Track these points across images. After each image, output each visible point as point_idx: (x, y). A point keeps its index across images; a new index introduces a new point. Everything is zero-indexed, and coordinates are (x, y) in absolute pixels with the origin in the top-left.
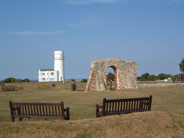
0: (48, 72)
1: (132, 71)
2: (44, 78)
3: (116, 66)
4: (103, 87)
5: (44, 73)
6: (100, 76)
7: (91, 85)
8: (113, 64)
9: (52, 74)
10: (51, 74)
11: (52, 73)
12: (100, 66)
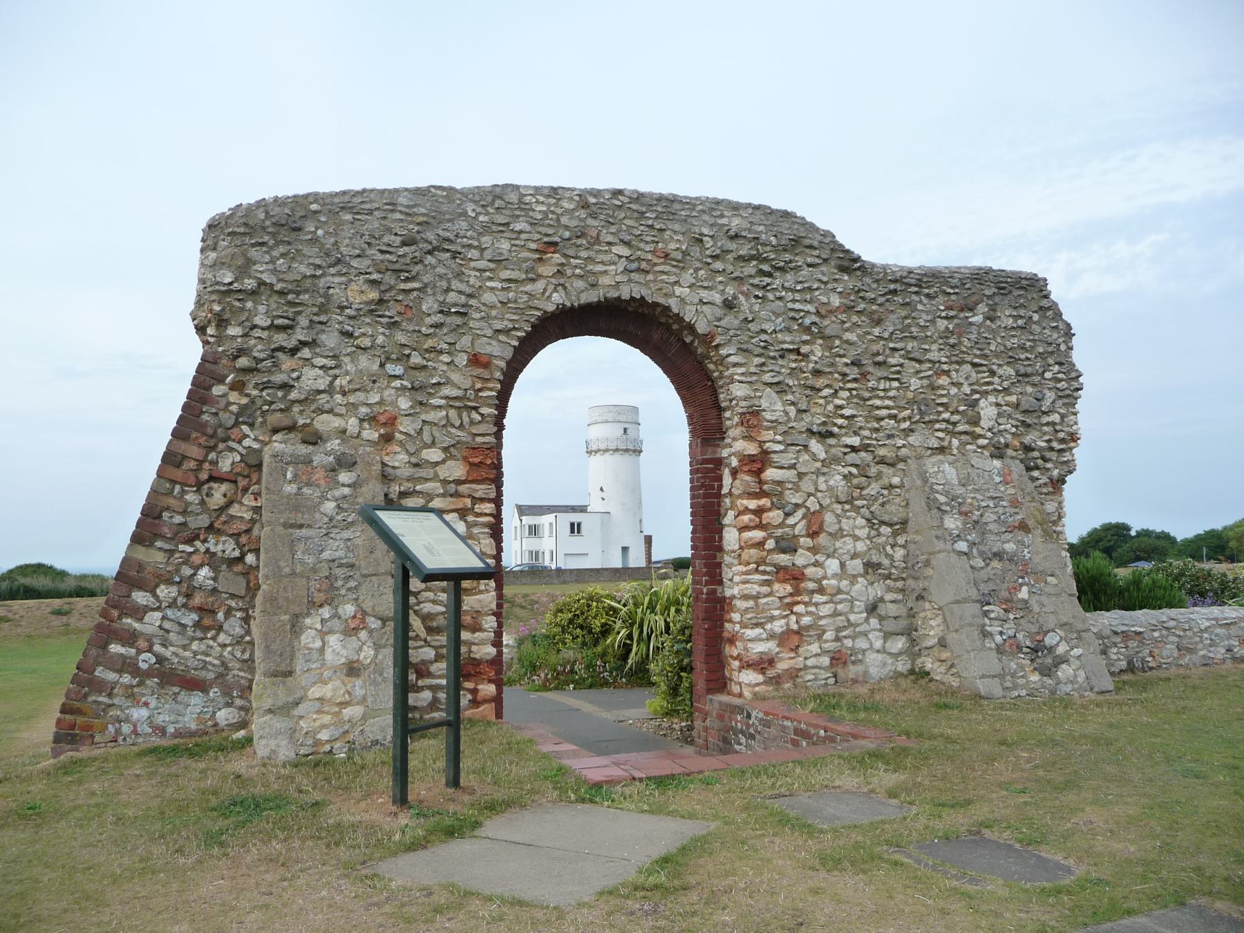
0: (550, 518)
1: (987, 411)
2: (537, 553)
3: (689, 315)
4: (352, 669)
5: (579, 525)
6: (344, 462)
7: (130, 638)
8: (638, 267)
9: (572, 531)
10: (583, 527)
11: (572, 525)
12: (358, 294)
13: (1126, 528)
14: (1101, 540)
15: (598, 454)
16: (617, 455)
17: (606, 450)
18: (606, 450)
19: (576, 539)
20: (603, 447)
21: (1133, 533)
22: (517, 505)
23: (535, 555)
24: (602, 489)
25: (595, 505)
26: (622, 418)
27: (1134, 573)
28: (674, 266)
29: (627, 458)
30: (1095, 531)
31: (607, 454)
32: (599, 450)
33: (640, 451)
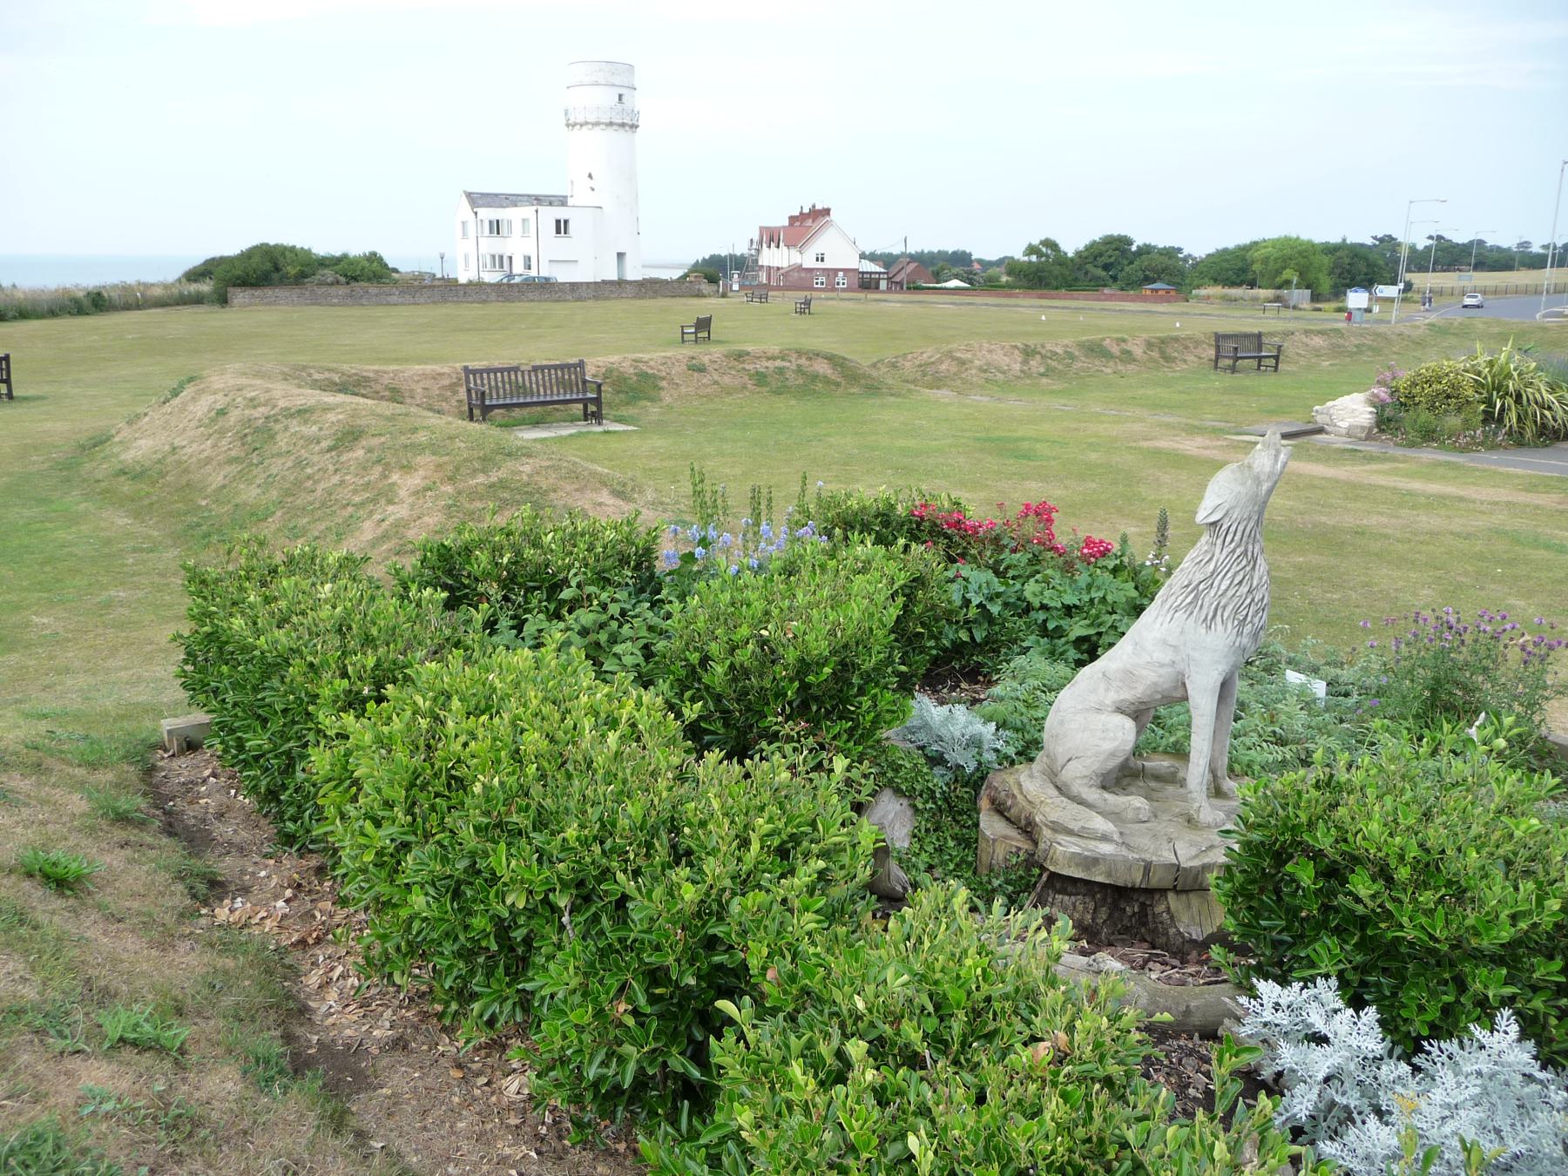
2: (501, 257)
5: (566, 222)
9: (558, 232)
11: (558, 222)
13: (1129, 242)
14: (1101, 255)
15: (585, 128)
16: (610, 130)
17: (597, 124)
18: (597, 124)
19: (562, 241)
20: (592, 119)
21: (1134, 248)
22: (465, 192)
23: (499, 261)
24: (590, 176)
25: (580, 196)
26: (617, 81)
27: (1302, 685)
28: (1290, 319)
29: (621, 136)
30: (1093, 244)
31: (597, 129)
32: (587, 123)
33: (637, 127)
